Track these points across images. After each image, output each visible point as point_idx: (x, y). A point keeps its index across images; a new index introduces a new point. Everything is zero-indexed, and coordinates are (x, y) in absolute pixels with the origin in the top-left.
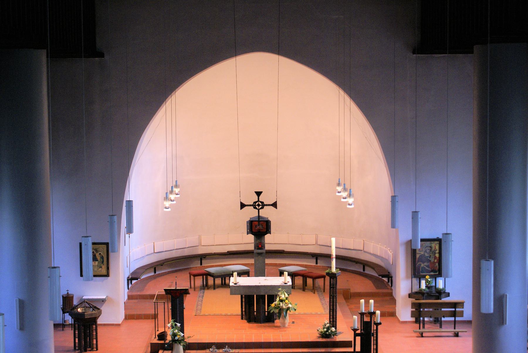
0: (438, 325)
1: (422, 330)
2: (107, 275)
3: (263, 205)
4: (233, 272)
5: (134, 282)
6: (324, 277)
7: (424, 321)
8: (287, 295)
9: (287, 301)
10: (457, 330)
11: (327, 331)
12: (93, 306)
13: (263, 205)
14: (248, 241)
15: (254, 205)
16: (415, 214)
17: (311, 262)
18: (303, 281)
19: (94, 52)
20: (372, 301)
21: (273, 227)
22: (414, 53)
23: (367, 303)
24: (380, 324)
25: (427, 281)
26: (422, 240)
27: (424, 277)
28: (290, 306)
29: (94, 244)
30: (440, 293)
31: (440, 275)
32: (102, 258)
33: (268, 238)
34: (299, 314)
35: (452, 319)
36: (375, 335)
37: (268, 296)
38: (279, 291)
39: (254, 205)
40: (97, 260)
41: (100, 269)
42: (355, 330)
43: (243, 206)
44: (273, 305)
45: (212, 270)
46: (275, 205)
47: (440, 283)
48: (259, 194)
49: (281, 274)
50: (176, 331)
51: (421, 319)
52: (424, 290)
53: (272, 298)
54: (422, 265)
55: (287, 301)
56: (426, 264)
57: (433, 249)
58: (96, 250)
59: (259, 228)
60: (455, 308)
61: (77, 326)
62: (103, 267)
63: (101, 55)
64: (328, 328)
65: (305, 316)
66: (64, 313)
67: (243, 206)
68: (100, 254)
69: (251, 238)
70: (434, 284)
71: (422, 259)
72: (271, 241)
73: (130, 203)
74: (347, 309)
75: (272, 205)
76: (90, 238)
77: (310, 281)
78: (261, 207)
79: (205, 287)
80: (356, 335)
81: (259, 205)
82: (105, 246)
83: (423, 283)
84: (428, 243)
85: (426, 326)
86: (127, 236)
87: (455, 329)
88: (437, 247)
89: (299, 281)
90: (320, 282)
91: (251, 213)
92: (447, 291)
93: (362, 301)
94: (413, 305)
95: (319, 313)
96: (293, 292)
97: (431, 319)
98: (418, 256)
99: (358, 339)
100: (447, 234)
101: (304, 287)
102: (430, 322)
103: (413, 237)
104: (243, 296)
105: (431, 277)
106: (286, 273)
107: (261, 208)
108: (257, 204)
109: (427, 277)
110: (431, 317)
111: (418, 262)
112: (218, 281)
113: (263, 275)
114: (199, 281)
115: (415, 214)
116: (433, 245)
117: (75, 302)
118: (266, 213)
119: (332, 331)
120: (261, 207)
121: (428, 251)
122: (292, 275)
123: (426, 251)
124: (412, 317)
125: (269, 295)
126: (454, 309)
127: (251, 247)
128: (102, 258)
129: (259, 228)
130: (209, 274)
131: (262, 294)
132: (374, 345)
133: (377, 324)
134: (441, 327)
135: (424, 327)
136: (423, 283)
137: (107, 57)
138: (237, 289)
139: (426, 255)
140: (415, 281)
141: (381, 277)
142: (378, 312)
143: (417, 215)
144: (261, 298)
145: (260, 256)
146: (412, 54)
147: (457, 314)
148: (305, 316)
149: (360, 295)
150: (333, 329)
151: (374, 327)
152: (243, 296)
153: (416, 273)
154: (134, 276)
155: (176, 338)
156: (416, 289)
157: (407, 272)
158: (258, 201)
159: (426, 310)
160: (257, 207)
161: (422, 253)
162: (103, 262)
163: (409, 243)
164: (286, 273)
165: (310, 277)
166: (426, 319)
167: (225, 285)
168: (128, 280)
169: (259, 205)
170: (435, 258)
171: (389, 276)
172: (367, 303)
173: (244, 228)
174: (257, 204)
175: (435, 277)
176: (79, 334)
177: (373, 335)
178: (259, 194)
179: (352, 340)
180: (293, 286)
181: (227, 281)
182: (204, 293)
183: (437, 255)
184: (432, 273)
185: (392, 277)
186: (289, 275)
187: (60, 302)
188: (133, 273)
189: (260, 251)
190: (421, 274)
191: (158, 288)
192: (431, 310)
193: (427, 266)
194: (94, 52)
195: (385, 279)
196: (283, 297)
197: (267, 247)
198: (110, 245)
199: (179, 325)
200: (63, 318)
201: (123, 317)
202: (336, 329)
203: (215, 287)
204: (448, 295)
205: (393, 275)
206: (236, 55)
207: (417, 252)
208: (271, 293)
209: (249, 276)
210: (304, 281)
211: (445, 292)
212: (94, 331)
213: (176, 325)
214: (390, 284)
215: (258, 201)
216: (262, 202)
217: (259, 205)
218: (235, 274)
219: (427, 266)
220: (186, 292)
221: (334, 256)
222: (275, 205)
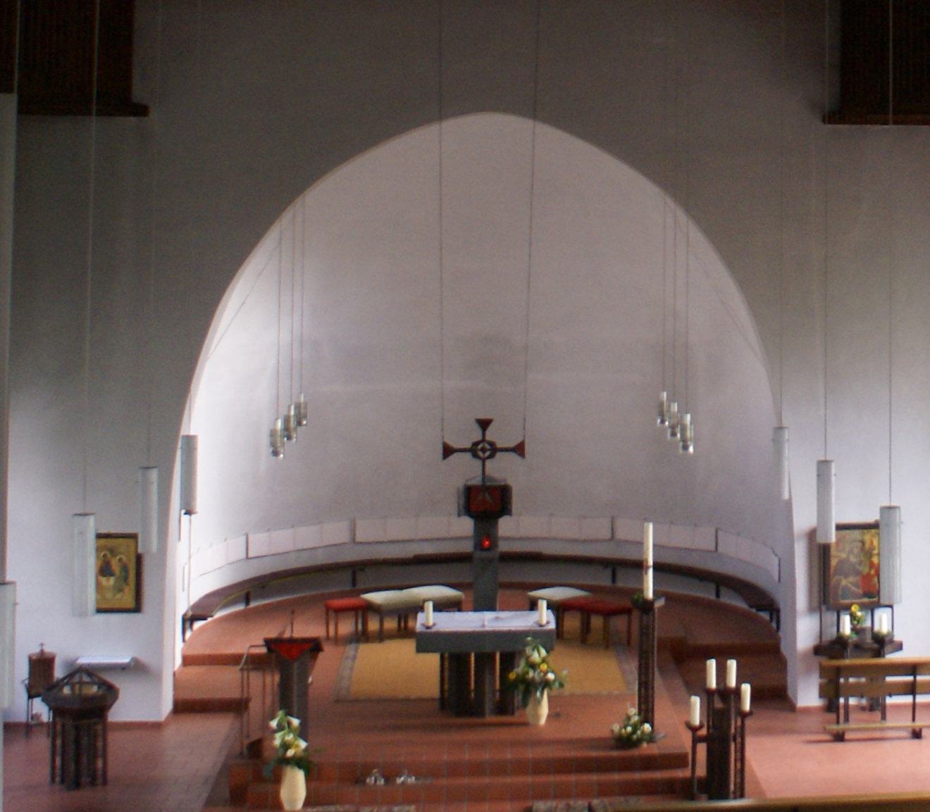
0: (878, 714)
1: (842, 726)
2: (137, 609)
3: (494, 450)
4: (425, 601)
5: (198, 625)
6: (628, 611)
7: (846, 706)
8: (543, 652)
9: (544, 667)
10: (918, 723)
11: (634, 732)
12: (100, 679)
13: (494, 450)
14: (476, 435)
15: (473, 450)
16: (823, 468)
17: (603, 579)
18: (583, 623)
19: (121, 102)
20: (732, 665)
21: (516, 502)
23: (722, 672)
25: (853, 617)
26: (840, 527)
27: (847, 608)
28: (551, 676)
29: (99, 536)
30: (881, 643)
33: (505, 526)
34: (572, 695)
35: (908, 699)
36: (739, 740)
37: (501, 655)
38: (526, 645)
39: (473, 450)
40: (112, 574)
41: (118, 596)
42: (694, 730)
43: (448, 451)
44: (512, 676)
45: (377, 597)
46: (519, 449)
47: (882, 622)
48: (484, 424)
49: (533, 606)
50: (290, 737)
51: (842, 700)
52: (849, 637)
53: (509, 660)
54: (844, 582)
55: (544, 667)
56: (852, 579)
57: (867, 545)
58: (113, 551)
59: (487, 503)
61: (59, 727)
62: (127, 590)
63: (141, 111)
64: (635, 727)
65: (580, 695)
66: (31, 697)
67: (448, 451)
68: (120, 560)
69: (466, 526)
70: (868, 624)
71: (843, 570)
72: (514, 530)
73: (190, 442)
74: (678, 682)
76: (91, 520)
77: (597, 621)
78: (488, 453)
79: (363, 637)
80: (696, 740)
81: (483, 450)
83: (846, 621)
84: (856, 534)
85: (852, 716)
86: (185, 518)
87: (914, 720)
89: (573, 622)
90: (619, 623)
91: (466, 470)
92: (897, 638)
93: (712, 664)
94: (823, 671)
95: (616, 692)
96: (559, 649)
97: (864, 702)
98: (834, 562)
99: (702, 749)
100: (890, 508)
101: (584, 639)
102: (863, 709)
103: (818, 521)
104: (446, 655)
105: (863, 607)
106: (543, 605)
107: (489, 457)
108: (480, 447)
109: (854, 608)
110: (862, 697)
111: (835, 574)
112: (391, 624)
113: (491, 607)
114: (346, 627)
115: (823, 468)
116: (867, 538)
117: (59, 673)
118: (502, 469)
119: (643, 732)
120: (488, 453)
121: (856, 551)
122: (558, 608)
123: (851, 551)
124: (821, 696)
125: (509, 648)
126: (910, 678)
127: (468, 547)
128: (125, 568)
129: (487, 503)
130: (370, 608)
131: (488, 650)
132: (736, 760)
133: (744, 716)
134: (884, 717)
135: (847, 720)
136: (846, 621)
137: (154, 114)
138: (427, 641)
139: (853, 559)
141: (754, 610)
142: (746, 689)
143: (829, 470)
144: (485, 660)
145: (487, 569)
147: (918, 690)
148: (580, 695)
149: (707, 653)
150: (647, 727)
151: (734, 723)
152: (446, 655)
153: (826, 598)
154: (199, 612)
155: (290, 753)
156: (831, 633)
158: (484, 461)
159: (851, 680)
160: (481, 454)
161: (844, 556)
162: (126, 579)
163: (812, 535)
164: (543, 605)
165: (598, 612)
166: (853, 701)
167: (404, 632)
168: (184, 620)
169: (483, 450)
171: (772, 608)
172: (722, 672)
173: (452, 501)
174: (480, 447)
175: (871, 608)
176: (64, 745)
177: (735, 740)
178: (484, 424)
179: (689, 750)
180: (559, 633)
181: (410, 623)
182: (357, 649)
184: (866, 600)
185: (778, 611)
186: (549, 607)
187: (23, 671)
188: (196, 606)
189: (485, 554)
190: (842, 601)
191: (251, 641)
192: (863, 680)
193: (851, 583)
194: (121, 102)
195: (765, 616)
196: (536, 657)
197: (504, 547)
198: (140, 539)
199: (296, 722)
200: (29, 708)
201: (167, 706)
202: (652, 726)
203: (381, 636)
204: (899, 647)
205: (782, 606)
206: (441, 116)
207: (833, 552)
209: (460, 610)
210: (585, 625)
211: (892, 641)
212: (100, 739)
213: (289, 723)
214: (774, 625)
215: (483, 440)
216: (492, 444)
217: (483, 450)
218: (430, 606)
219: (851, 583)
220: (314, 646)
221: (651, 562)
222: (519, 449)
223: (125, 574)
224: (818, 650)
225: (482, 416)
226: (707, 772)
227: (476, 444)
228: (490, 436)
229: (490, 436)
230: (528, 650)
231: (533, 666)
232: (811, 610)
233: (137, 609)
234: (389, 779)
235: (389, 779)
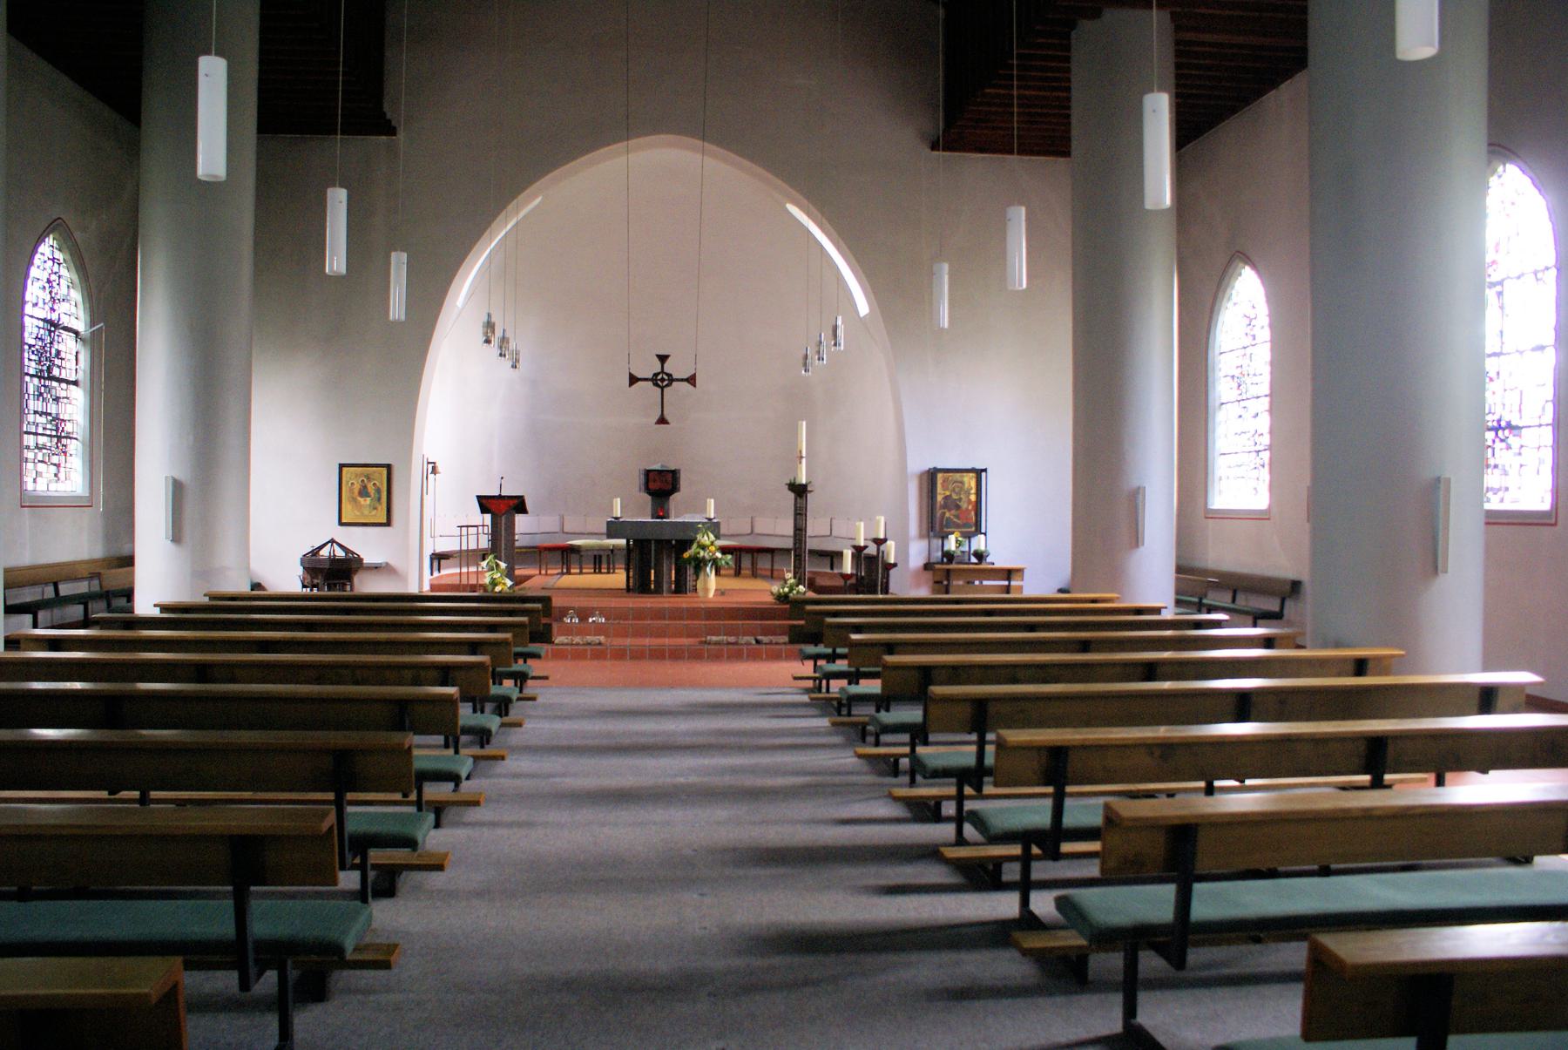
2: (388, 523)
8: (712, 537)
14: (640, 512)
19: (371, 119)
21: (683, 483)
22: (934, 147)
24: (895, 565)
31: (978, 531)
32: (379, 491)
39: (654, 380)
43: (633, 380)
44: (686, 555)
46: (692, 380)
47: (979, 543)
48: (663, 359)
50: (497, 576)
53: (686, 544)
60: (1009, 579)
75: (687, 380)
82: (384, 471)
88: (973, 484)
98: (939, 498)
128: (379, 491)
137: (401, 135)
140: (937, 542)
146: (928, 150)
155: (498, 589)
157: (920, 526)
170: (969, 502)
175: (969, 536)
178: (663, 359)
183: (973, 498)
199: (503, 565)
208: (681, 536)
216: (669, 375)
223: (373, 488)
224: (928, 566)
225: (662, 353)
226: (1141, 102)
227: (656, 375)
228: (668, 367)
229: (668, 367)
230: (699, 537)
231: (704, 547)
232: (921, 536)
233: (388, 523)
234: (583, 618)
235: (583, 618)
